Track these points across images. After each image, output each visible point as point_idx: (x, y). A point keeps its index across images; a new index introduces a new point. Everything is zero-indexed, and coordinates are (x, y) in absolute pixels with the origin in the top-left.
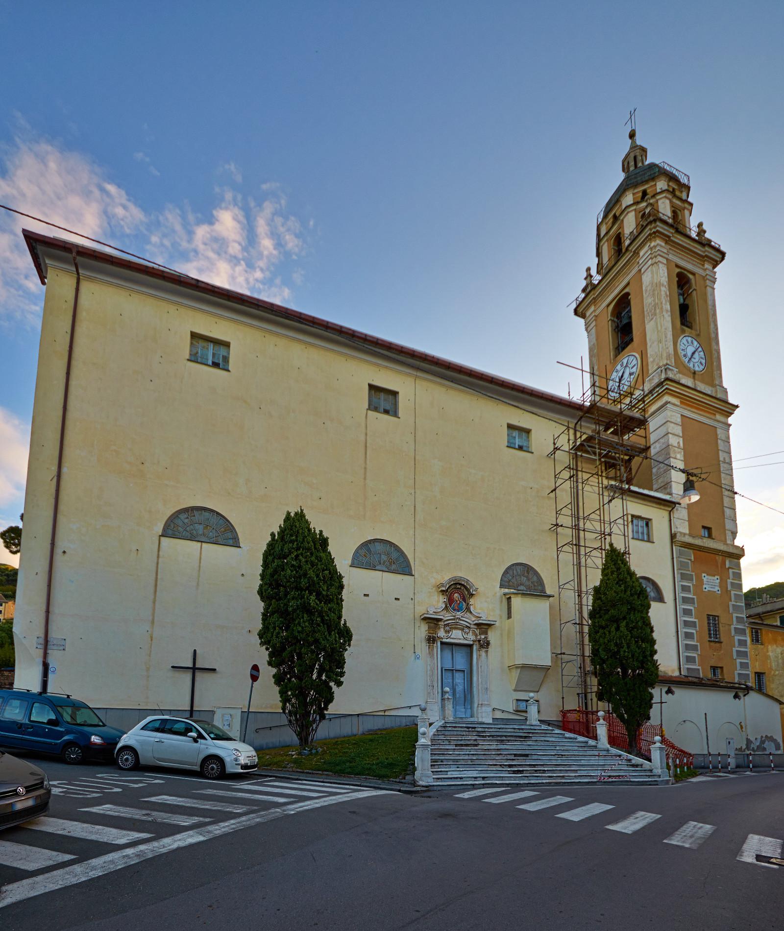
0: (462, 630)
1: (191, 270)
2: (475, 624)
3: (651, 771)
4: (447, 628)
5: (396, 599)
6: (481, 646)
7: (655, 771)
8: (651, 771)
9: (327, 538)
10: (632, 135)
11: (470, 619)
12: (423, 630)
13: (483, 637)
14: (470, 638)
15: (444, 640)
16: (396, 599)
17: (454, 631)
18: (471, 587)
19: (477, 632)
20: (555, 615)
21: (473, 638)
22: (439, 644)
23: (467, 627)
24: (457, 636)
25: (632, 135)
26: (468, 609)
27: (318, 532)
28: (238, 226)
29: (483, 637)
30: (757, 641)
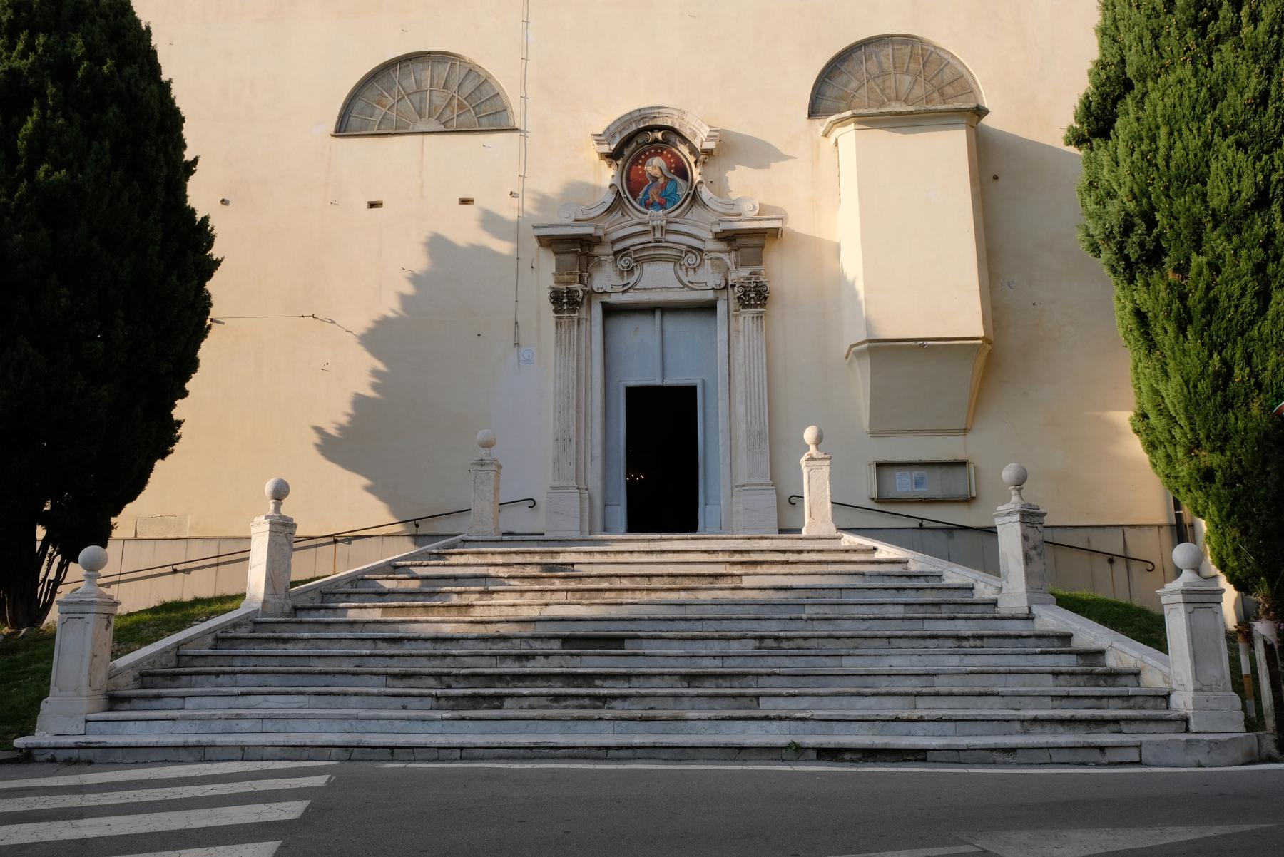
0: (677, 260)
3: (994, 603)
4: (624, 262)
6: (744, 301)
7: (1005, 607)
8: (994, 603)
9: (217, 263)
10: (280, 492)
11: (699, 226)
12: (546, 272)
13: (745, 272)
14: (705, 280)
15: (615, 299)
17: (649, 268)
19: (729, 259)
20: (993, 164)
21: (714, 279)
22: (597, 311)
23: (691, 249)
24: (658, 282)
25: (280, 492)
26: (695, 198)
27: (199, 217)
29: (745, 272)
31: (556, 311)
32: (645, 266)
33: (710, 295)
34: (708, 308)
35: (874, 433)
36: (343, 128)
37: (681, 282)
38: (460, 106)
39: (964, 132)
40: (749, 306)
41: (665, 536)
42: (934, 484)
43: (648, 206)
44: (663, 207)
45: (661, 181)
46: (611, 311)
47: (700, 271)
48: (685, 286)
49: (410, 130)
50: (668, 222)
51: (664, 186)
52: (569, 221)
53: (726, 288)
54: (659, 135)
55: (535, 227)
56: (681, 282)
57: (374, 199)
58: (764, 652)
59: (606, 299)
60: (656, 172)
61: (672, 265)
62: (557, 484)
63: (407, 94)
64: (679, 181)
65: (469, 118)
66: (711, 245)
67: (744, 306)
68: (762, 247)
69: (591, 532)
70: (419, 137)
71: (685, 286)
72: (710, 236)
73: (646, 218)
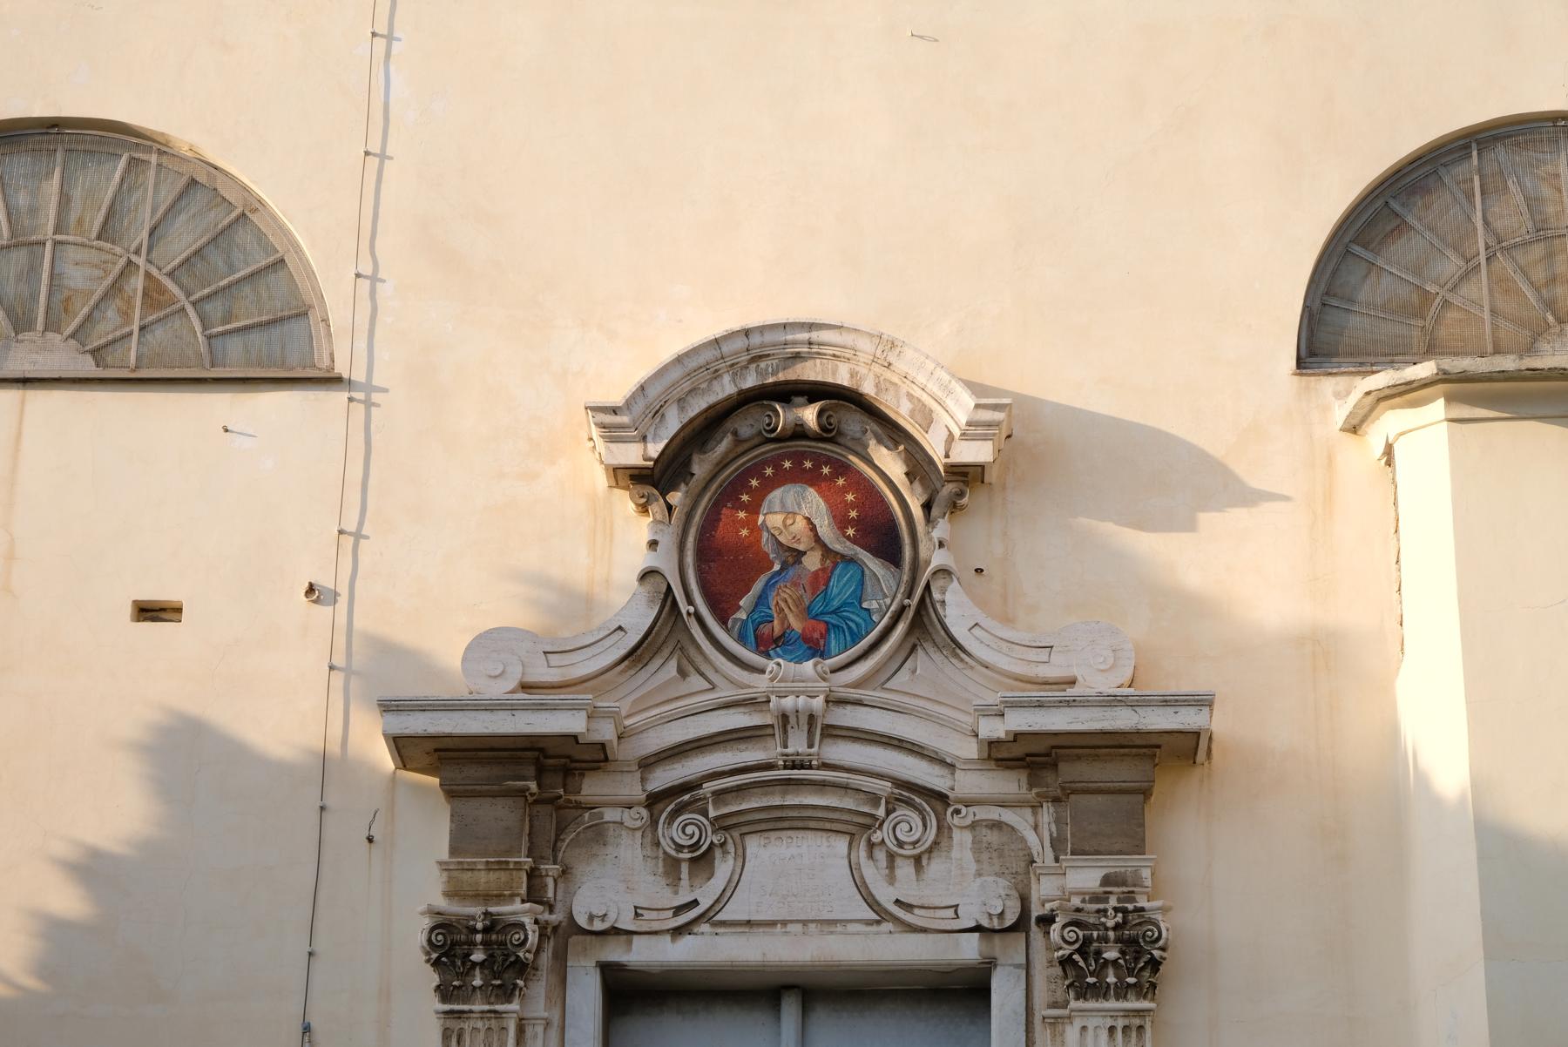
0: (859, 828)
1: (1106, 797)
2: (1000, 755)
4: (677, 833)
5: (148, 612)
6: (1082, 974)
11: (939, 716)
13: (1085, 877)
14: (957, 895)
15: (647, 954)
16: (148, 612)
18: (927, 420)
19: (1033, 829)
21: (984, 897)
22: (586, 994)
23: (909, 792)
26: (922, 623)
28: (990, 774)
29: (1085, 877)
30: (954, 474)
31: (444, 992)
32: (753, 845)
33: (969, 950)
37: (872, 902)
38: (154, 295)
43: (767, 644)
44: (816, 649)
45: (812, 562)
47: (935, 867)
50: (834, 701)
51: (820, 581)
52: (499, 689)
53: (1021, 925)
54: (809, 415)
56: (872, 902)
59: (614, 953)
61: (841, 844)
64: (873, 564)
71: (882, 915)
73: (760, 684)
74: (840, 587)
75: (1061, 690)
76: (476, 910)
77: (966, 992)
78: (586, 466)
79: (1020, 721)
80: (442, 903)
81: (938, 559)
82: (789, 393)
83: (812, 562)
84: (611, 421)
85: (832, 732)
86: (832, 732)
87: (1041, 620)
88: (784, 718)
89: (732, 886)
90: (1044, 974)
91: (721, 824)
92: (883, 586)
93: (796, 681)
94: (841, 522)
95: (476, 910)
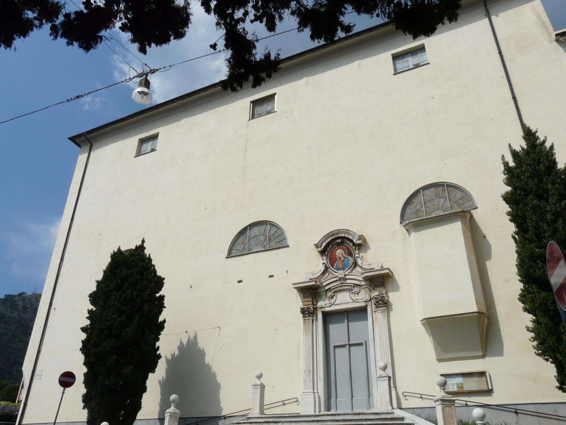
12: (297, 302)
14: (362, 297)
15: (327, 309)
22: (320, 316)
23: (355, 285)
24: (343, 301)
26: (355, 264)
31: (303, 317)
32: (338, 294)
33: (363, 304)
34: (363, 310)
35: (439, 360)
36: (229, 256)
37: (352, 300)
38: (270, 239)
39: (460, 222)
40: (380, 307)
41: (466, 354)
42: (472, 384)
43: (338, 269)
44: (344, 269)
45: (342, 258)
46: (326, 315)
47: (360, 294)
48: (354, 301)
49: (253, 251)
50: (345, 275)
51: (344, 260)
52: (307, 280)
53: (370, 300)
54: (340, 240)
55: (294, 284)
56: (352, 300)
57: (239, 280)
58: (514, 407)
59: (323, 310)
60: (340, 256)
61: (348, 293)
62: (305, 391)
63: (258, 237)
64: (350, 257)
65: (273, 244)
66: (363, 283)
67: (377, 307)
68: (384, 282)
69: (329, 409)
70: (255, 254)
71: (354, 301)
72: (361, 279)
73: (337, 274)
74: (346, 261)
75: (372, 270)
76: (305, 307)
77: (363, 310)
78: (315, 253)
79: (365, 275)
80: (302, 307)
81: (357, 255)
82: (338, 238)
83: (342, 258)
84: (317, 246)
85: (346, 279)
86: (346, 279)
87: (372, 260)
88: (340, 278)
89: (336, 300)
90: (373, 306)
91: (334, 292)
92: (351, 260)
93: (341, 273)
94: (345, 253)
95: (305, 307)
